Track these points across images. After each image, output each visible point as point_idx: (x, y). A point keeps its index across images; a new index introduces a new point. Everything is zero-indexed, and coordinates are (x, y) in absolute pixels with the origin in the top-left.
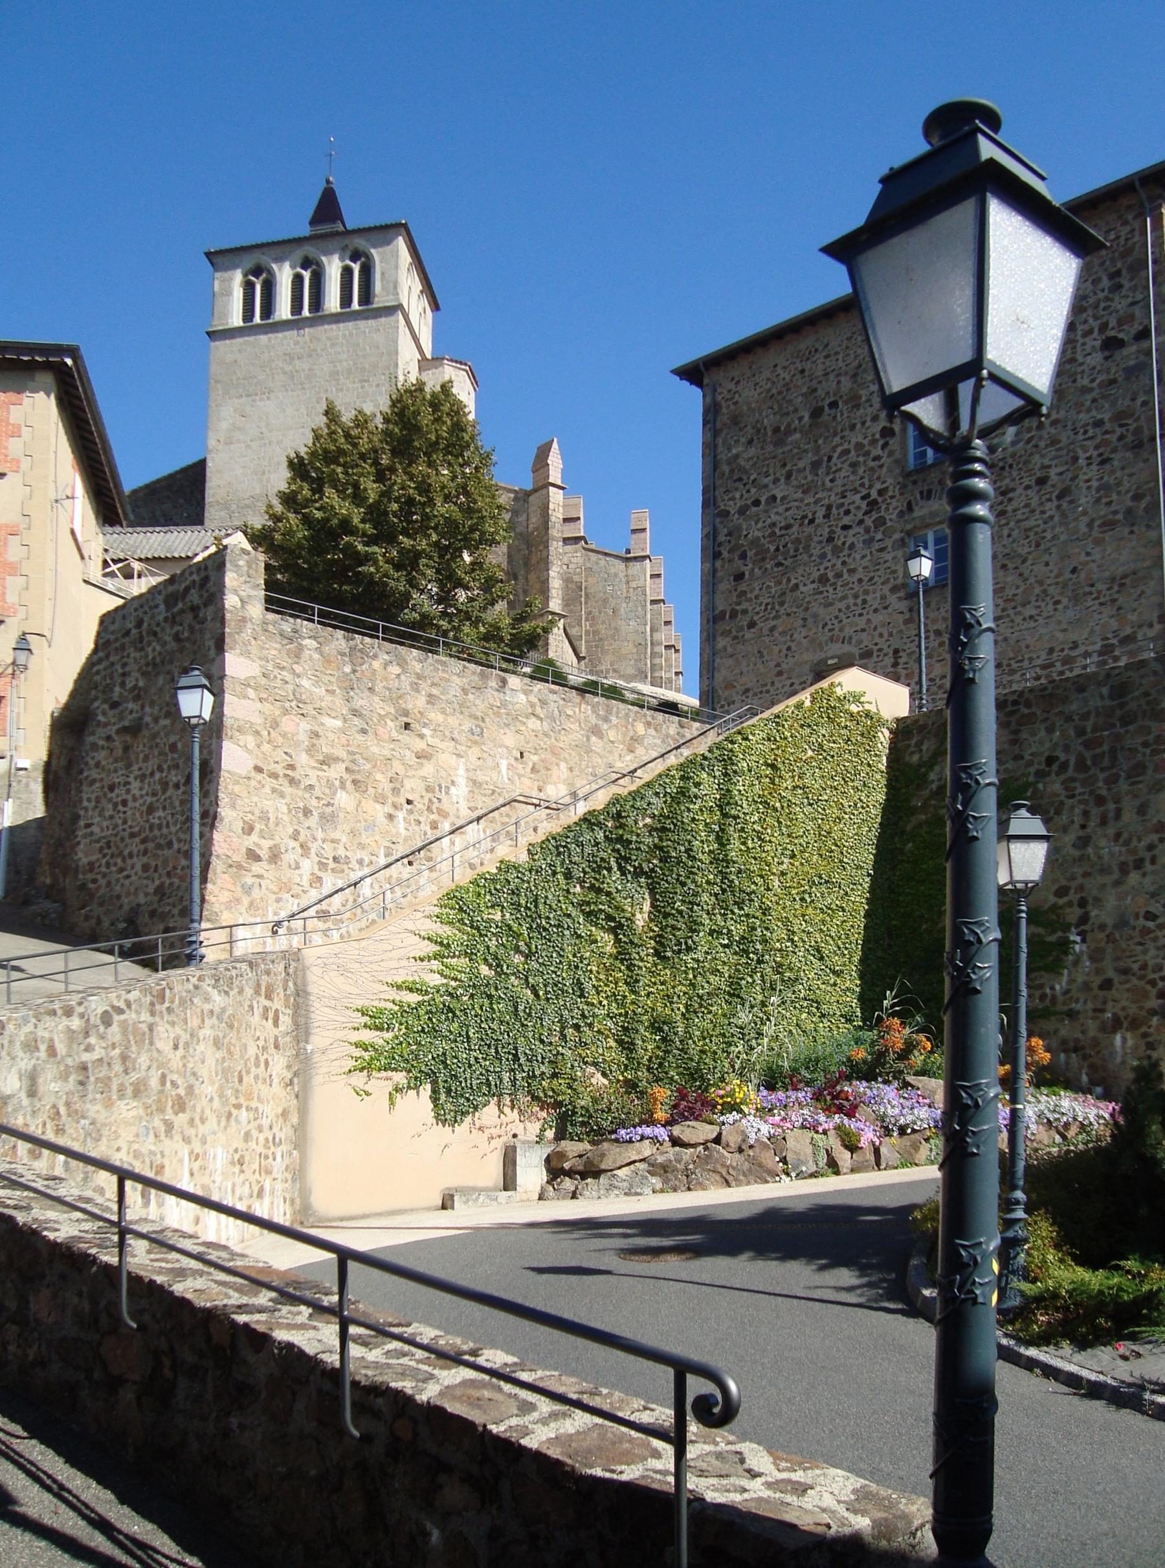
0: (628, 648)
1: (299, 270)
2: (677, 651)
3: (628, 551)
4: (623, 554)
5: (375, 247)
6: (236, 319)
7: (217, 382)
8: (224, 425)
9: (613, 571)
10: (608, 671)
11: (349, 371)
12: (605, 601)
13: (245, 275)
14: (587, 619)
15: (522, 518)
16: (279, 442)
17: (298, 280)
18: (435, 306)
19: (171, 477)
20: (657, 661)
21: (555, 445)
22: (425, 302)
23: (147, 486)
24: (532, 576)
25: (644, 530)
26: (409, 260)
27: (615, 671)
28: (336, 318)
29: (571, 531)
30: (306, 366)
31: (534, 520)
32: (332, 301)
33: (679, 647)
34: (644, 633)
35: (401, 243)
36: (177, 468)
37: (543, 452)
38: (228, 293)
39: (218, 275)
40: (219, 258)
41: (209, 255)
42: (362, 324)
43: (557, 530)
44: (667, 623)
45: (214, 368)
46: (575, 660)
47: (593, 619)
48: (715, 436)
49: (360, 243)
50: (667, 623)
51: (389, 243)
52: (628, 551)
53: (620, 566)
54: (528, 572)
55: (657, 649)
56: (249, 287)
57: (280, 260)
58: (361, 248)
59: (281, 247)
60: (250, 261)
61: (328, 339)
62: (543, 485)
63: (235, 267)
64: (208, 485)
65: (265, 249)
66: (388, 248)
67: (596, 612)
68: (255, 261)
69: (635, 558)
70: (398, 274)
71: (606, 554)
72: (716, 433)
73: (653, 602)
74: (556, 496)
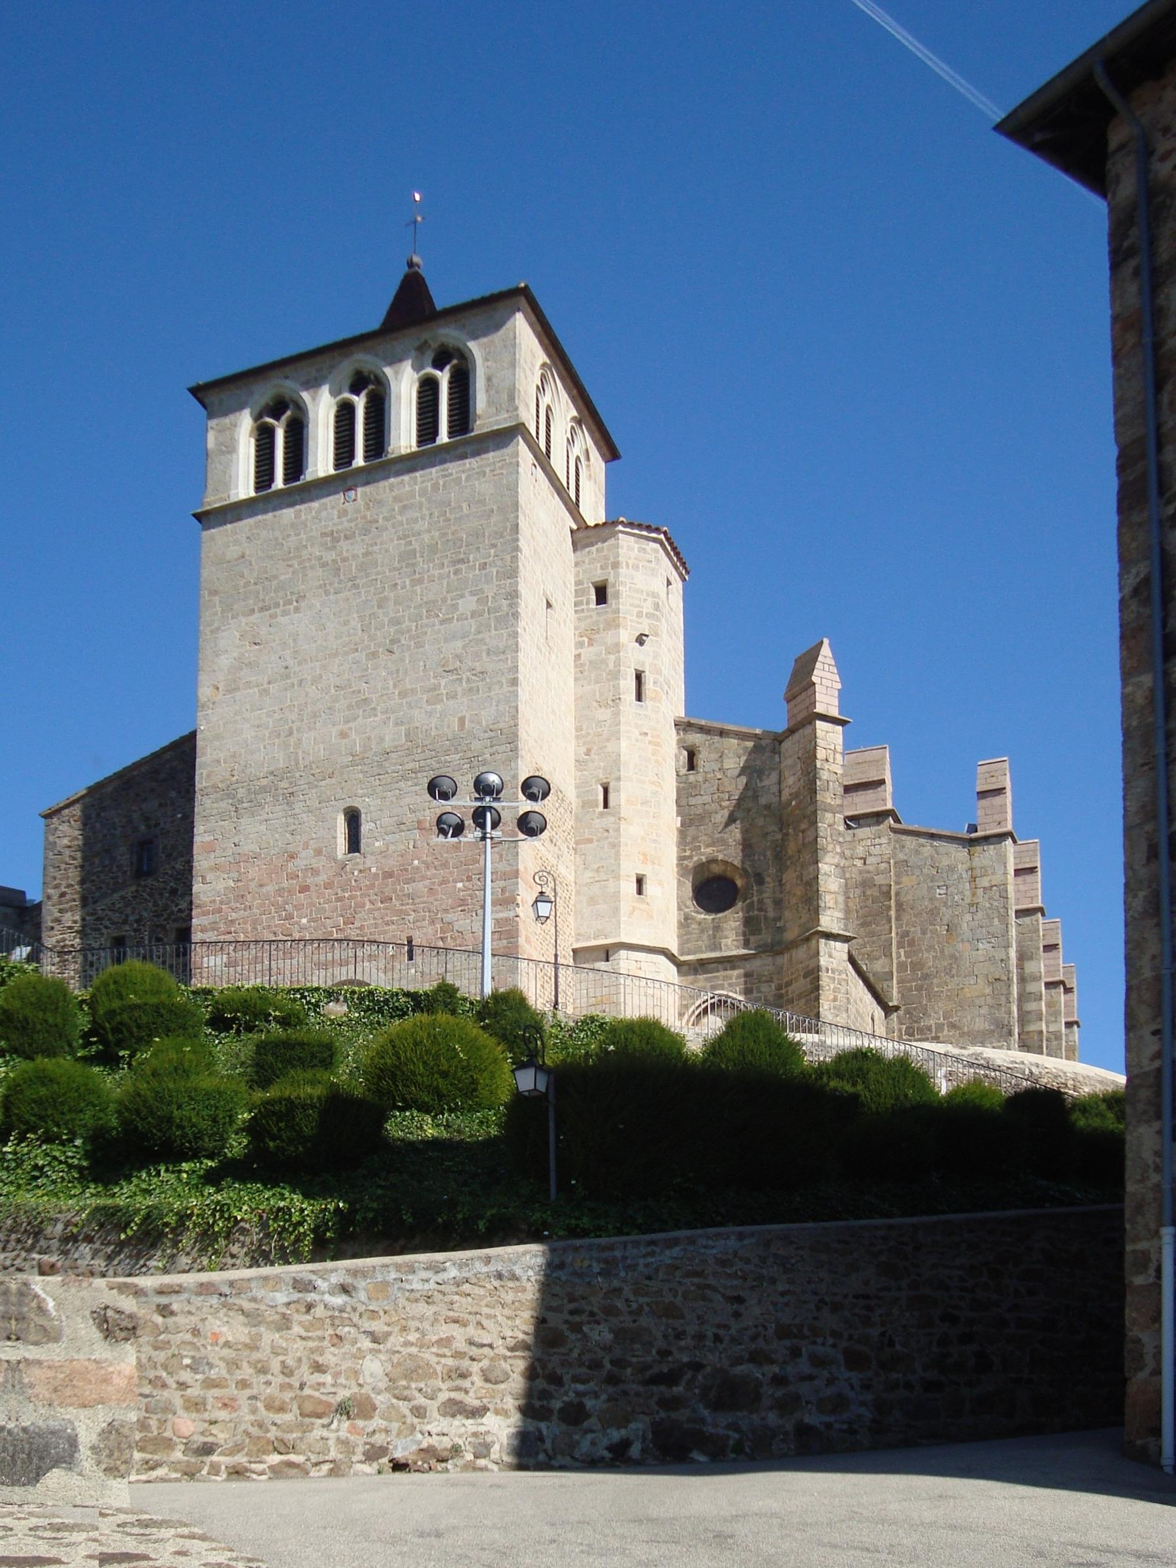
0: (976, 988)
1: (347, 395)
2: (1068, 990)
3: (973, 828)
4: (963, 833)
5: (475, 337)
6: (244, 487)
7: (215, 593)
8: (224, 661)
9: (945, 862)
10: (940, 1027)
11: (433, 549)
12: (933, 913)
13: (257, 417)
14: (900, 945)
15: (770, 780)
16: (317, 680)
17: (345, 413)
18: (611, 452)
19: (156, 756)
20: (1031, 1006)
21: (826, 651)
22: (585, 441)
23: (119, 776)
24: (789, 876)
25: (1000, 791)
26: (542, 357)
27: (953, 1026)
28: (410, 463)
29: (863, 803)
30: (359, 550)
31: (791, 781)
32: (403, 435)
33: (1073, 983)
34: (1005, 960)
35: (521, 326)
36: (165, 743)
37: (807, 662)
38: (230, 448)
39: (212, 423)
40: (213, 395)
41: (196, 391)
42: (453, 467)
43: (829, 796)
44: (1049, 948)
45: (207, 573)
46: (879, 1013)
47: (912, 943)
48: (1155, 288)
49: (448, 334)
50: (1049, 948)
51: (498, 327)
52: (973, 828)
53: (959, 854)
54: (782, 869)
55: (1031, 987)
56: (264, 438)
57: (313, 384)
58: (451, 342)
59: (313, 362)
60: (264, 393)
61: (396, 499)
62: (806, 719)
63: (241, 408)
64: (199, 761)
65: (288, 370)
66: (497, 337)
67: (916, 932)
68: (268, 391)
69: (986, 839)
70: (516, 368)
71: (932, 836)
72: (1156, 279)
73: (1020, 913)
74: (829, 737)
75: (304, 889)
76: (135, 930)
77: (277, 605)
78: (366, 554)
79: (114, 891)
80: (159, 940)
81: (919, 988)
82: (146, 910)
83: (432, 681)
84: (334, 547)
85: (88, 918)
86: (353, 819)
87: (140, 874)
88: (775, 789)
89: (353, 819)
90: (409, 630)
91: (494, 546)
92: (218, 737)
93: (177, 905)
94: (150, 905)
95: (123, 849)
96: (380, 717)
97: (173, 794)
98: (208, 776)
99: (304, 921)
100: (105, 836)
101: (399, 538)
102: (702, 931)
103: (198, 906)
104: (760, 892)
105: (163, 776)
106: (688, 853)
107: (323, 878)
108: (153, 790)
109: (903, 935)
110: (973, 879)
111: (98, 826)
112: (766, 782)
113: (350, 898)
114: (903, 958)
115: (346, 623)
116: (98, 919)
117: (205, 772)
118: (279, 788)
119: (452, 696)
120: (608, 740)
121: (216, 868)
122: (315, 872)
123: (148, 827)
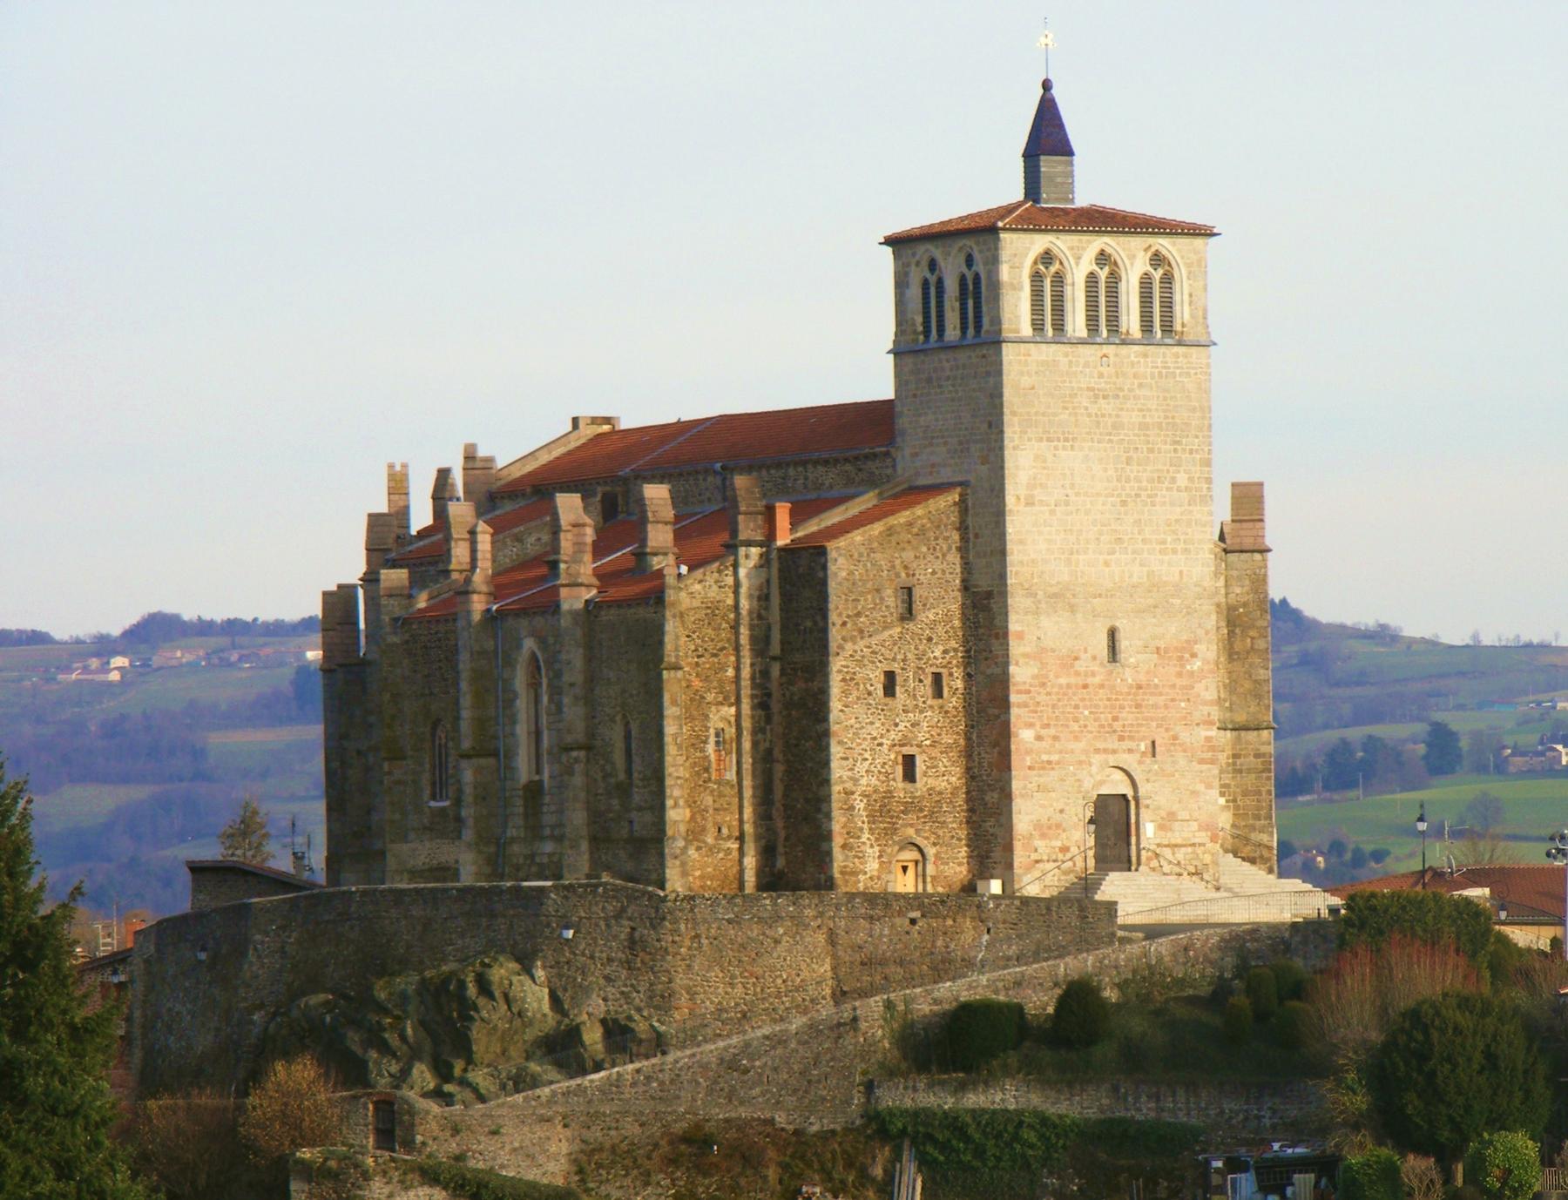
11: (1160, 426)
75: (1085, 686)
79: (885, 628)
89: (1112, 634)
92: (1021, 542)
95: (889, 592)
97: (924, 549)
105: (915, 530)
107: (1097, 680)
115: (1106, 470)
118: (1061, 599)
119: (1174, 551)
121: (1026, 656)
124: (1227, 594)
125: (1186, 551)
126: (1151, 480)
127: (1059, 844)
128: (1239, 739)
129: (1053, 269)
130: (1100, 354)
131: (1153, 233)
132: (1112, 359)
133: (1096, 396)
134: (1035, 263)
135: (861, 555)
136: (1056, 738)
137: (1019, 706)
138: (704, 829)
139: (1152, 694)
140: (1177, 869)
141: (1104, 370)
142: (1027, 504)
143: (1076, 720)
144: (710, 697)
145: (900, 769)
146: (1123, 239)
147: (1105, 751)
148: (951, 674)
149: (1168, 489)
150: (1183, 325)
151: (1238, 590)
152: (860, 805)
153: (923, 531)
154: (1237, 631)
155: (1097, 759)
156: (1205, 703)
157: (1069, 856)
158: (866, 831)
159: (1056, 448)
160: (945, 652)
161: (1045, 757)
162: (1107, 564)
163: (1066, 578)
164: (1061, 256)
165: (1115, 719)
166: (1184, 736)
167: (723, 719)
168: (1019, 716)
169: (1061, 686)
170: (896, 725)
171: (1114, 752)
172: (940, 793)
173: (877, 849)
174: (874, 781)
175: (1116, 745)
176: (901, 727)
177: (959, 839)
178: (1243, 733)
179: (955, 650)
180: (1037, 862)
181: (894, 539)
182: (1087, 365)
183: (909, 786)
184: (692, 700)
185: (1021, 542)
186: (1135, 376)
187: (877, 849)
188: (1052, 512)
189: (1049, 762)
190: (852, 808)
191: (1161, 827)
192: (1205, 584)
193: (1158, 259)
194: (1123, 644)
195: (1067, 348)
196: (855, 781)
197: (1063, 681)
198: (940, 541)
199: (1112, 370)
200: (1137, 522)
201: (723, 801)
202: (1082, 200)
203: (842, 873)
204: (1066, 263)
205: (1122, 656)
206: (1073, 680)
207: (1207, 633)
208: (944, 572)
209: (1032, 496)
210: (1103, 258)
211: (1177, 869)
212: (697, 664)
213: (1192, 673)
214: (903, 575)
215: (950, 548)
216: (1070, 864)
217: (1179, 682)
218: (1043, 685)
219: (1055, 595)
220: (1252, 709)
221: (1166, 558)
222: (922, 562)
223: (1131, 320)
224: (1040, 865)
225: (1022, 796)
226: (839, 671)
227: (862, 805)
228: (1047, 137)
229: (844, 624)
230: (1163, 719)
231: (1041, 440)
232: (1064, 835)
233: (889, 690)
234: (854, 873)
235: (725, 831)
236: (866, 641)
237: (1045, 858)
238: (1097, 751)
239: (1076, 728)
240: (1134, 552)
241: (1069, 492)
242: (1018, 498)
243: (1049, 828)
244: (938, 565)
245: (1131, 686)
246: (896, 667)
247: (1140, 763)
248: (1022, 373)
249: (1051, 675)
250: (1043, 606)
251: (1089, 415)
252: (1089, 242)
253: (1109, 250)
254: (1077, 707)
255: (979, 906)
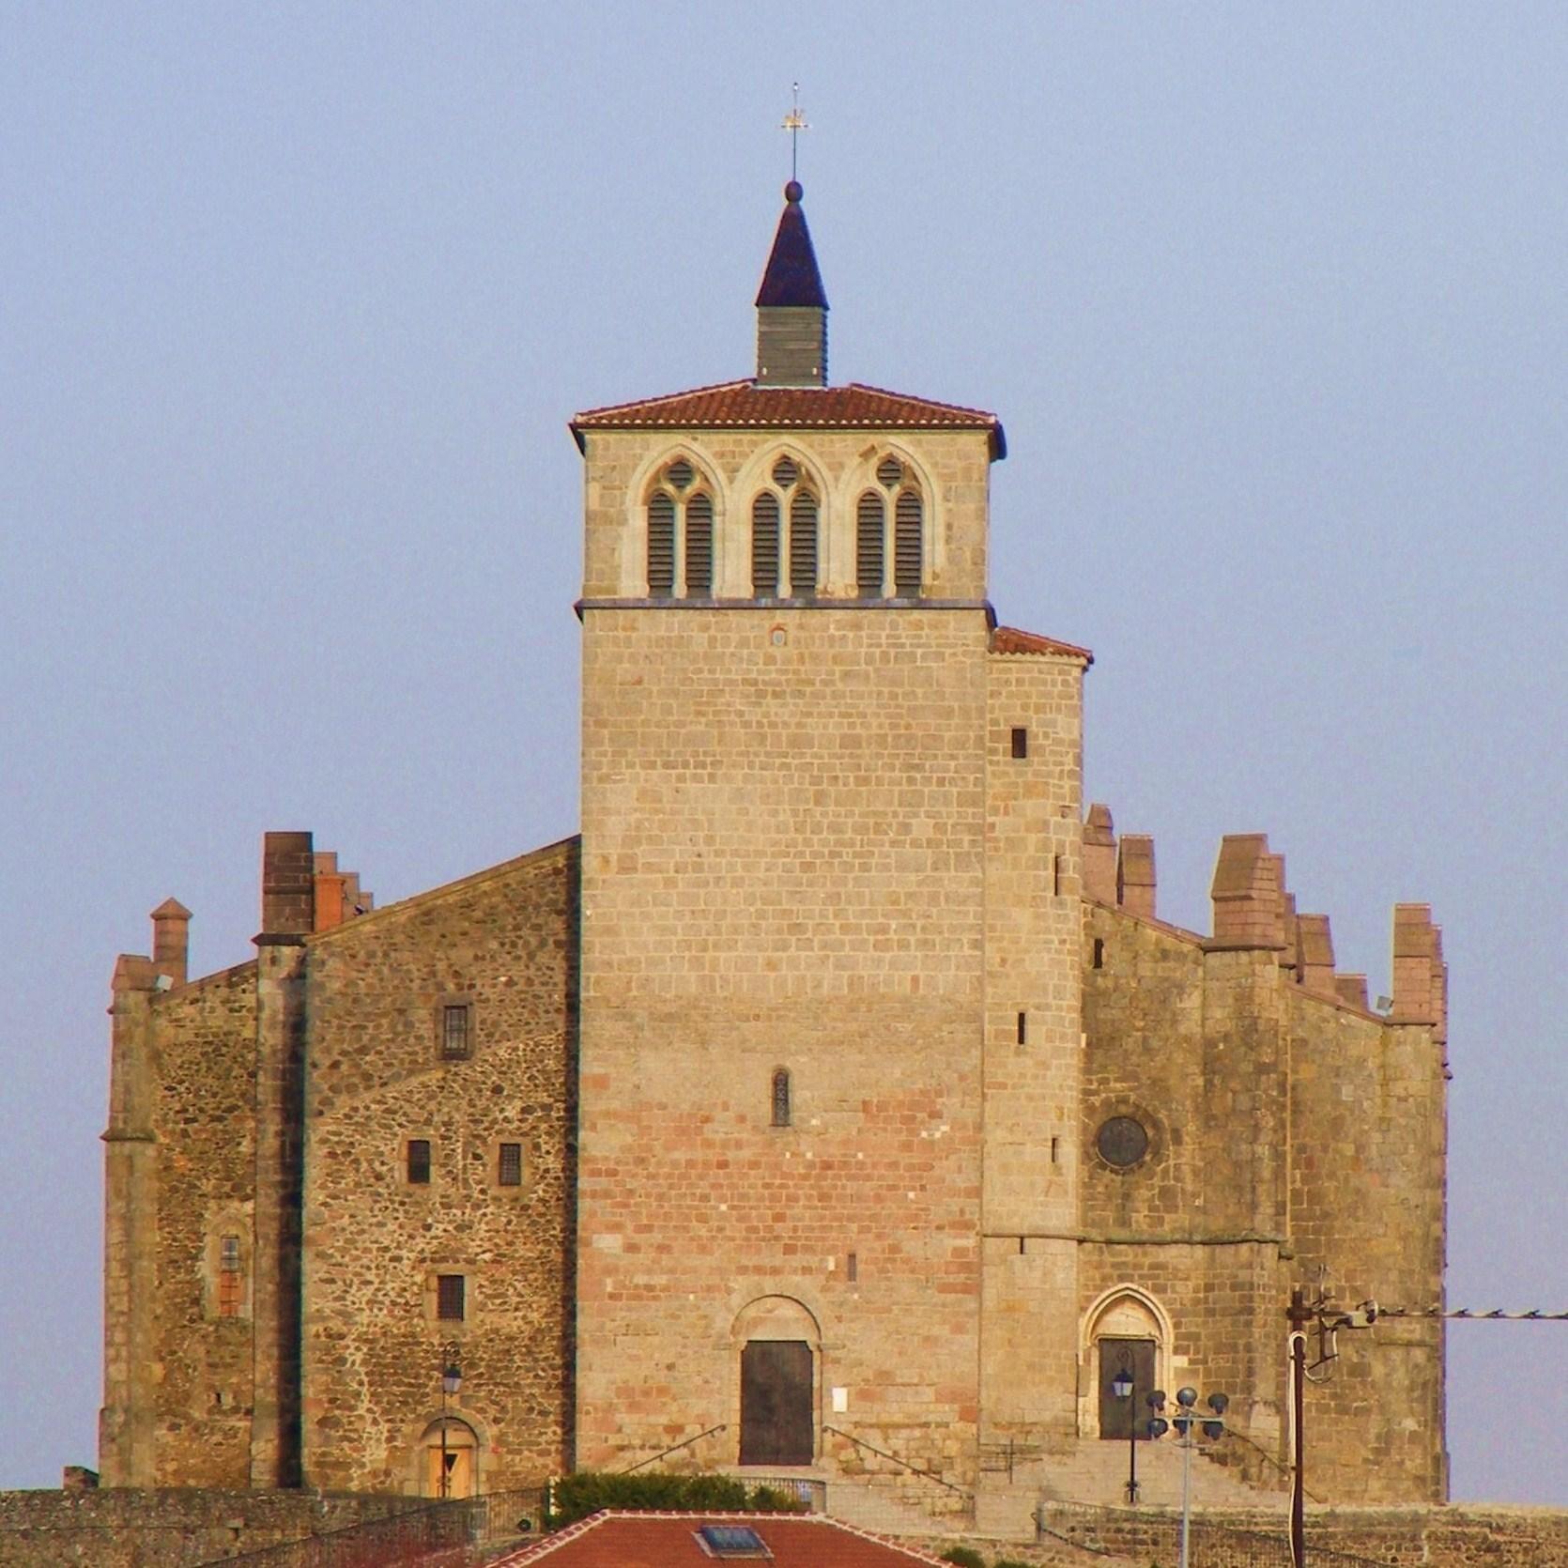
14: (1296, 1165)
75: (723, 1165)
76: (443, 1138)
77: (686, 765)
78: (799, 725)
79: (411, 1073)
80: (477, 1157)
81: (1317, 1231)
82: (458, 1109)
83: (881, 920)
84: (759, 704)
85: (373, 1106)
86: (781, 1083)
87: (449, 1056)
88: (1197, 1015)
89: (781, 1083)
90: (853, 845)
91: (953, 757)
92: (609, 931)
93: (502, 1111)
94: (464, 1103)
95: (423, 1013)
96: (818, 953)
97: (494, 945)
98: (597, 982)
99: (723, 1207)
100: (396, 987)
101: (842, 715)
102: (1109, 1198)
103: (587, 1161)
104: (1178, 1155)
105: (478, 914)
106: (1094, 1087)
107: (746, 1154)
108: (464, 934)
109: (1301, 1149)
110: (1385, 1083)
111: (385, 970)
112: (1186, 1004)
113: (782, 1186)
114: (1298, 1185)
115: (775, 813)
116: (387, 1111)
117: (593, 975)
118: (679, 1021)
119: (903, 945)
120: (1027, 951)
121: (608, 1114)
122: (739, 1145)
123: (460, 987)
124: (1204, 1019)
125: (924, 943)
126: (861, 829)
127: (664, 1420)
128: (1212, 1258)
129: (690, 490)
130: (767, 625)
131: (871, 427)
132: (792, 632)
133: (761, 694)
134: (656, 479)
135: (372, 955)
136: (663, 1248)
137: (594, 1195)
138: (187, 1396)
139: (851, 1178)
140: (892, 1465)
141: (778, 652)
142: (623, 870)
143: (703, 1219)
144: (207, 1186)
145: (432, 1301)
146: (817, 437)
147: (759, 1270)
148: (537, 1147)
149: (893, 843)
150: (935, 576)
151: (1218, 1014)
152: (355, 1356)
153: (491, 913)
154: (1217, 1080)
155: (740, 1284)
156: (954, 1193)
157: (680, 1440)
158: (366, 1397)
159: (681, 779)
160: (524, 1110)
161: (641, 1279)
162: (771, 965)
163: (693, 989)
164: (703, 467)
165: (779, 1218)
166: (913, 1246)
167: (237, 1221)
168: (593, 1214)
169: (675, 1164)
170: (428, 1228)
171: (775, 1271)
172: (511, 1338)
173: (385, 1427)
174: (383, 1317)
175: (779, 1260)
176: (438, 1230)
177: (543, 1413)
178: (1218, 1249)
179: (547, 1108)
180: (622, 1448)
181: (435, 930)
182: (744, 643)
183: (449, 1326)
184: (174, 1190)
185: (609, 931)
186: (836, 659)
187: (385, 1427)
188: (670, 883)
189: (649, 1288)
190: (342, 1361)
191: (862, 1395)
192: (960, 997)
193: (891, 470)
194: (798, 1096)
195: (709, 617)
196: (346, 1315)
197: (680, 1155)
198: (525, 932)
199: (792, 651)
200: (834, 898)
201: (226, 1352)
202: (838, 378)
203: (319, 1464)
204: (712, 480)
205: (795, 1117)
206: (699, 1155)
207: (962, 1078)
208: (530, 982)
209: (633, 857)
210: (786, 470)
211: (892, 1465)
212: (185, 1133)
213: (930, 1144)
214: (451, 986)
215: (543, 944)
216: (684, 1452)
217: (905, 1159)
218: (641, 1161)
219: (670, 1017)
220: (1231, 1211)
221: (888, 955)
222: (487, 965)
223: (837, 566)
224: (628, 1455)
225: (595, 1342)
226: (324, 1141)
227: (359, 1357)
228: (792, 279)
229: (335, 1065)
230: (874, 1218)
231: (653, 765)
232: (674, 1408)
233: (418, 1172)
234: (342, 1465)
235: (228, 1401)
236: (376, 1093)
237: (637, 1442)
238: (743, 1270)
239: (703, 1233)
240: (824, 946)
241: (703, 848)
242: (606, 860)
243: (646, 1393)
244: (518, 971)
245: (811, 1165)
246: (430, 1133)
247: (824, 1289)
248: (619, 659)
249: (658, 1146)
250: (648, 1034)
251: (747, 725)
252: (755, 444)
253: (795, 457)
254: (705, 1198)
255: (312, 1510)
